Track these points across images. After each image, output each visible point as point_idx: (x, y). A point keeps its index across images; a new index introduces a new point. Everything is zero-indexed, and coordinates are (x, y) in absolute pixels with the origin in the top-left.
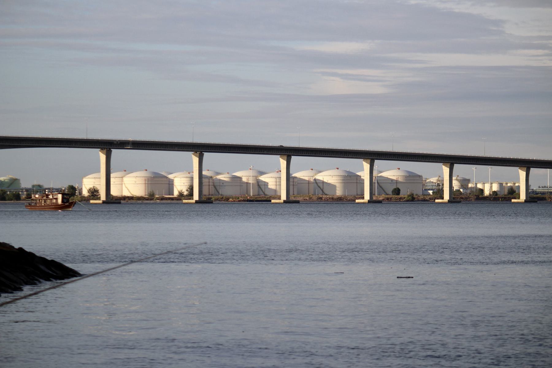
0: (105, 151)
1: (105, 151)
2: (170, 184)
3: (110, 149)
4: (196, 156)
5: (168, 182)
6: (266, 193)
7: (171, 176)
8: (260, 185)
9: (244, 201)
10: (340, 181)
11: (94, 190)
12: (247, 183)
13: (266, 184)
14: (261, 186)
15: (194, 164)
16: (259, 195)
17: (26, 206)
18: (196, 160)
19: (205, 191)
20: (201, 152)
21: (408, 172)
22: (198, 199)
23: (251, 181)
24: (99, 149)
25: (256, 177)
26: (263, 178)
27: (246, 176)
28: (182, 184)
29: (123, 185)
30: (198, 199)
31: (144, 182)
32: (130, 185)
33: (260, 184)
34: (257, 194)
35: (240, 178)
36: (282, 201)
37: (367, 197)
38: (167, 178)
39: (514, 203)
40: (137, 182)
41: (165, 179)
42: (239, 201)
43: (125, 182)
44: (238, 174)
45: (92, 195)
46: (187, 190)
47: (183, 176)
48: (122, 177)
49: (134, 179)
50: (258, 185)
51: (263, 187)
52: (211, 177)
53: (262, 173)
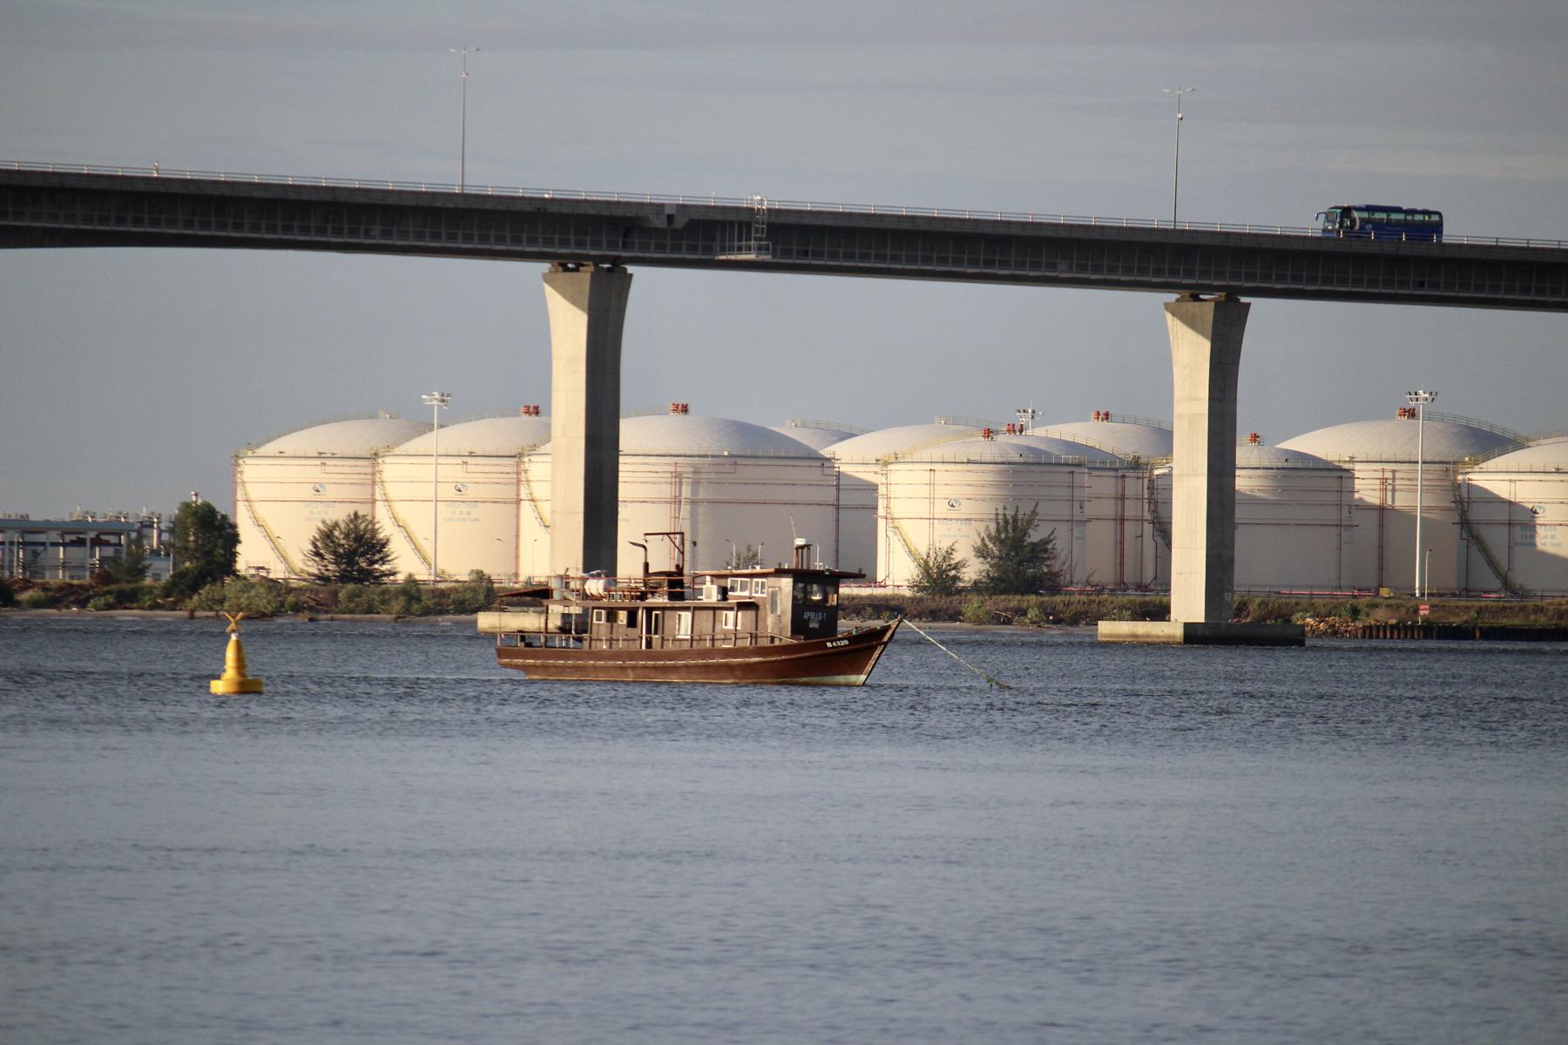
0: (585, 277)
1: (585, 277)
2: (855, 507)
3: (617, 262)
4: (1192, 323)
5: (831, 495)
6: (1520, 579)
7: (852, 458)
8: (1482, 528)
9: (1403, 630)
10: (992, 491)
11: (359, 538)
12: (1381, 509)
13: (1521, 520)
14: (1487, 534)
15: (1179, 374)
16: (1467, 592)
17: (501, 653)
18: (1190, 353)
19: (1250, 574)
20: (1232, 295)
21: (744, 430)
22: (1199, 616)
23: (1412, 498)
24: (545, 267)
25: (1448, 467)
26: (1496, 478)
27: (1376, 457)
28: (942, 509)
29: (525, 506)
30: (1199, 616)
31: (666, 491)
32: (471, 503)
33: (1476, 514)
34: (1451, 582)
35: (1340, 475)
36: (1171, 629)
37: (1189, 601)
38: (825, 462)
39: (490, 636)
40: (472, 492)
41: (814, 474)
42: (1370, 632)
43: (393, 491)
44: (1322, 444)
45: (344, 578)
46: (982, 552)
47: (948, 451)
48: (521, 455)
49: (452, 471)
50: (1465, 523)
51: (1496, 539)
52: (1136, 465)
53: (1490, 443)
